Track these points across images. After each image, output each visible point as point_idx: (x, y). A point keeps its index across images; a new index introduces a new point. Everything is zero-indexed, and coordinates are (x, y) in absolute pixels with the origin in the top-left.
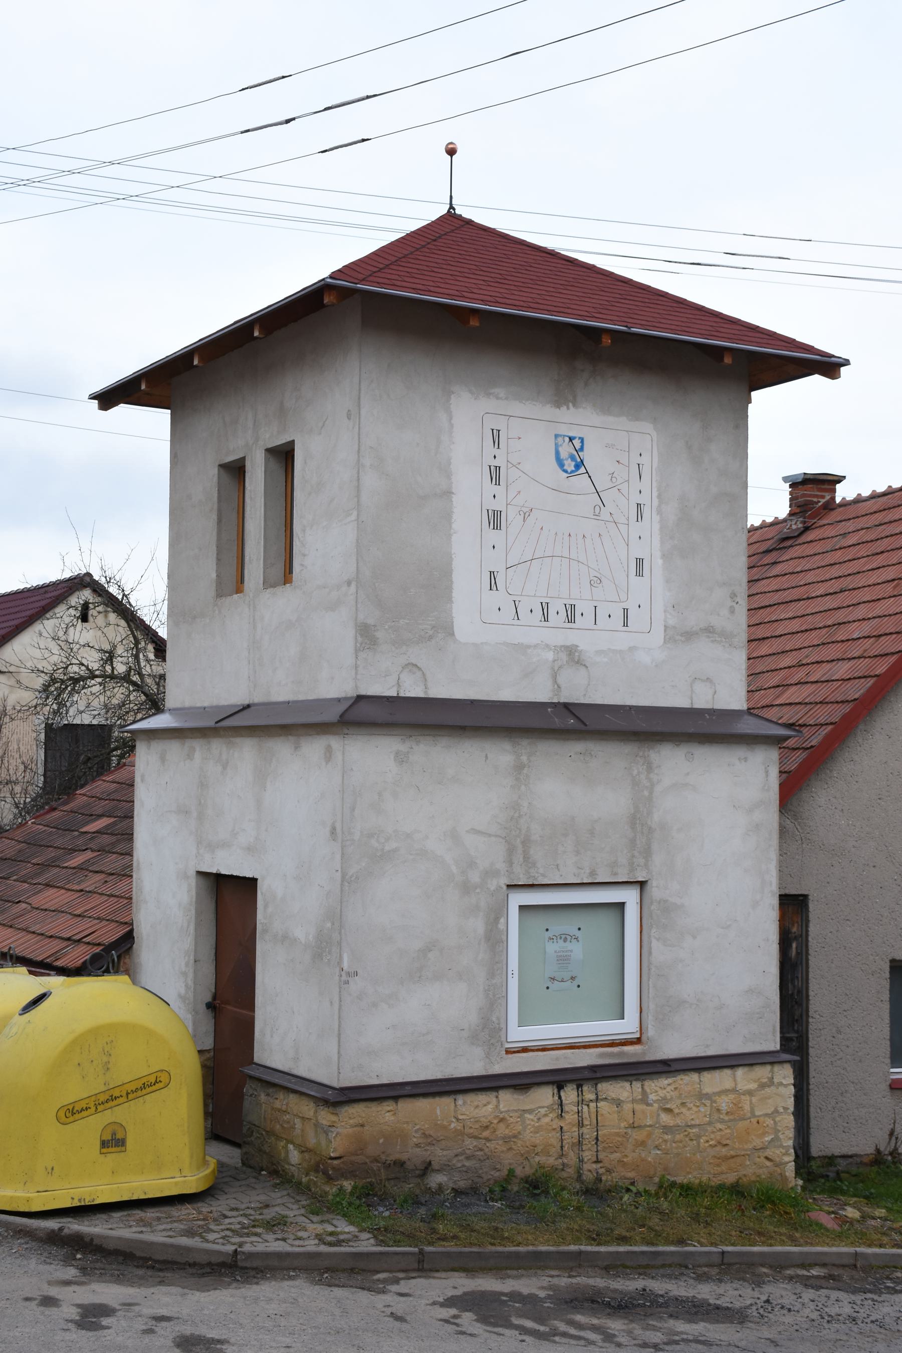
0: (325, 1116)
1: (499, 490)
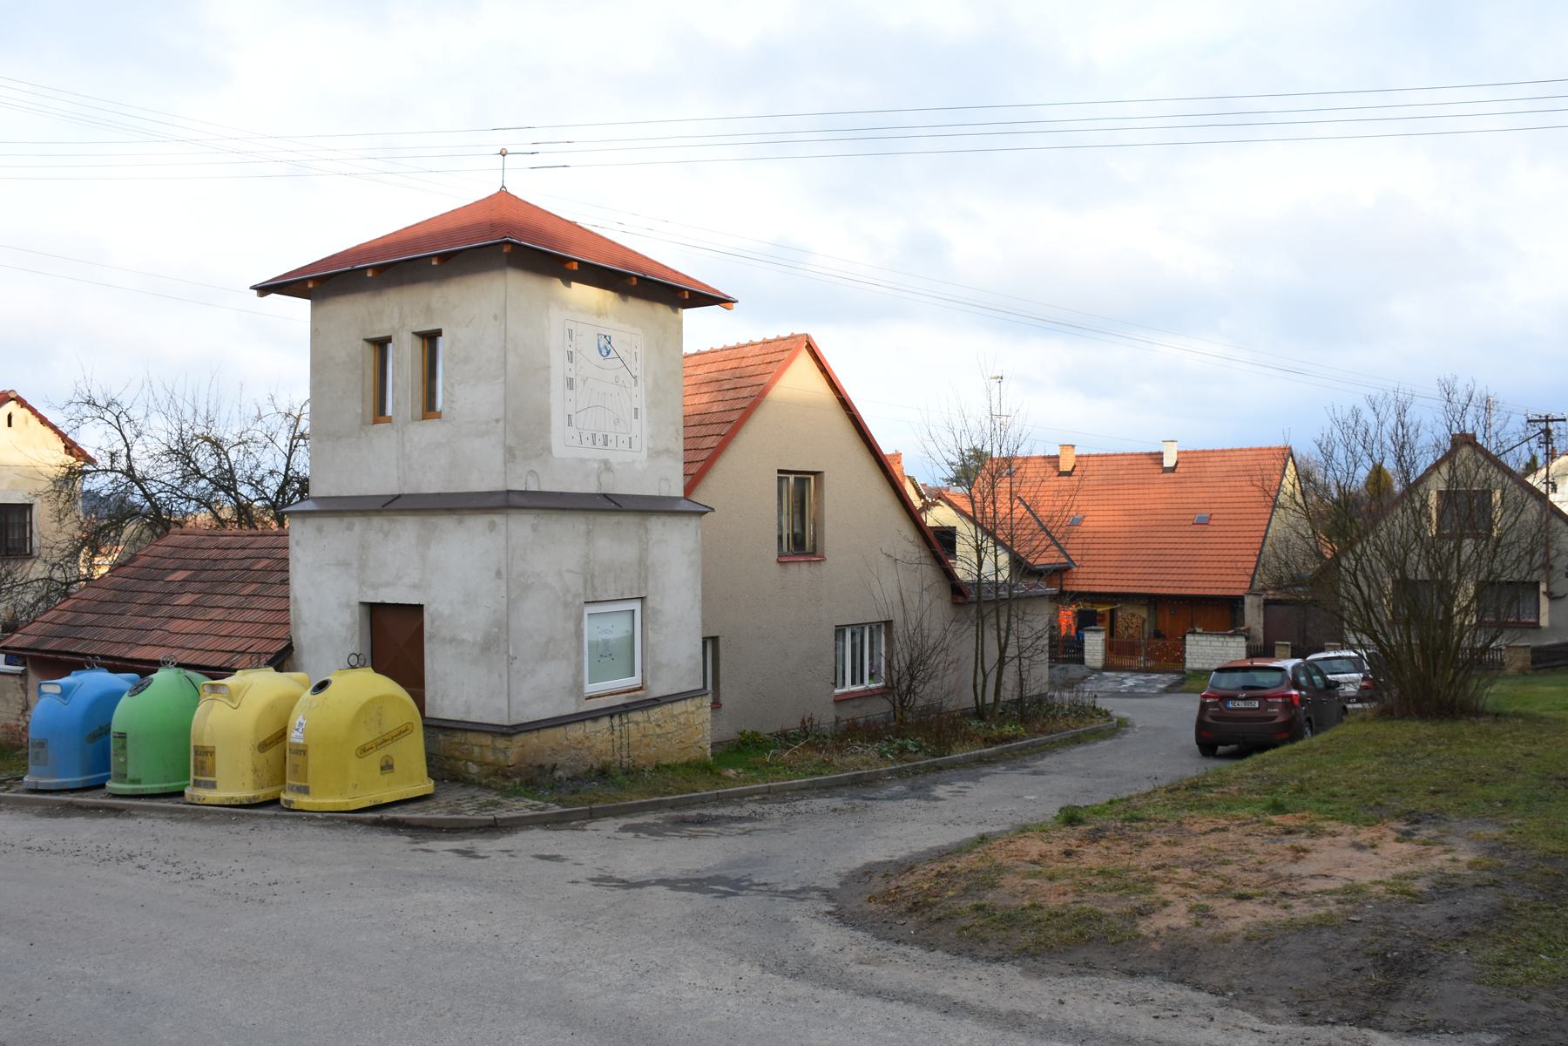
0: (501, 743)
1: (572, 366)
